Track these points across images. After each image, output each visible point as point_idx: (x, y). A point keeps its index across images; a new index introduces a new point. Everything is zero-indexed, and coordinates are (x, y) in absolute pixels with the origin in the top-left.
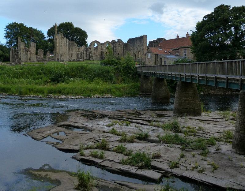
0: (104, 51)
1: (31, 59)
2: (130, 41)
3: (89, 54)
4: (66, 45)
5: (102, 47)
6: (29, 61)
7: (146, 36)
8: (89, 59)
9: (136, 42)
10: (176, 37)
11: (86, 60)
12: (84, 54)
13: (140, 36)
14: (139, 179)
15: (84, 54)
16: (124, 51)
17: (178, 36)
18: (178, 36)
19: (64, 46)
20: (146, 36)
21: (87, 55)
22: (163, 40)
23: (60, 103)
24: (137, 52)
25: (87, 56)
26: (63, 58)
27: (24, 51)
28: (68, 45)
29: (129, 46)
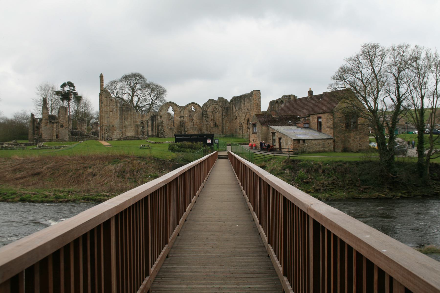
0: (186, 120)
1: (59, 135)
2: (235, 99)
3: (158, 126)
4: (115, 110)
5: (182, 113)
6: (55, 138)
7: (259, 91)
8: (158, 136)
9: (243, 102)
10: (307, 95)
11: (152, 136)
12: (148, 126)
13: (248, 92)
14: (138, 195)
15: (148, 126)
16: (222, 119)
17: (310, 92)
18: (310, 92)
19: (111, 113)
20: (259, 91)
21: (154, 128)
22: (292, 98)
23: (104, 137)
24: (246, 122)
25: (154, 131)
26: (108, 133)
27: (48, 121)
28: (118, 111)
29: (232, 110)
